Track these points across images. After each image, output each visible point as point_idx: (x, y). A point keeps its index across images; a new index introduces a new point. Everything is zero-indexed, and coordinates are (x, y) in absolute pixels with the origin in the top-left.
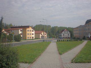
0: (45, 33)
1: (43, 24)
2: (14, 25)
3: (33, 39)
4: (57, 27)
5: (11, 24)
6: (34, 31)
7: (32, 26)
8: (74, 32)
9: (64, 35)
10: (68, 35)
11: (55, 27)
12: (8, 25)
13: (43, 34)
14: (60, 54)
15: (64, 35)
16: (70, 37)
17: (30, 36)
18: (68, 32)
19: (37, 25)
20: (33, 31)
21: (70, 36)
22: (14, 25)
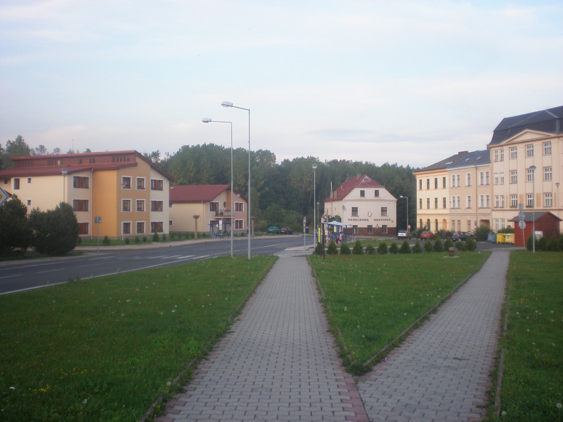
0: (235, 199)
1: (225, 140)
2: (42, 147)
3: (156, 239)
4: (312, 160)
5: (20, 139)
6: (166, 185)
7: (156, 155)
8: (506, 149)
9: (355, 211)
10: (384, 210)
11: (299, 162)
12: (14, 142)
13: (221, 207)
14: (358, 370)
15: (355, 211)
16: (392, 224)
17: (156, 217)
18: (384, 193)
19: (260, 151)
20: (157, 186)
21: (391, 221)
22: (42, 147)
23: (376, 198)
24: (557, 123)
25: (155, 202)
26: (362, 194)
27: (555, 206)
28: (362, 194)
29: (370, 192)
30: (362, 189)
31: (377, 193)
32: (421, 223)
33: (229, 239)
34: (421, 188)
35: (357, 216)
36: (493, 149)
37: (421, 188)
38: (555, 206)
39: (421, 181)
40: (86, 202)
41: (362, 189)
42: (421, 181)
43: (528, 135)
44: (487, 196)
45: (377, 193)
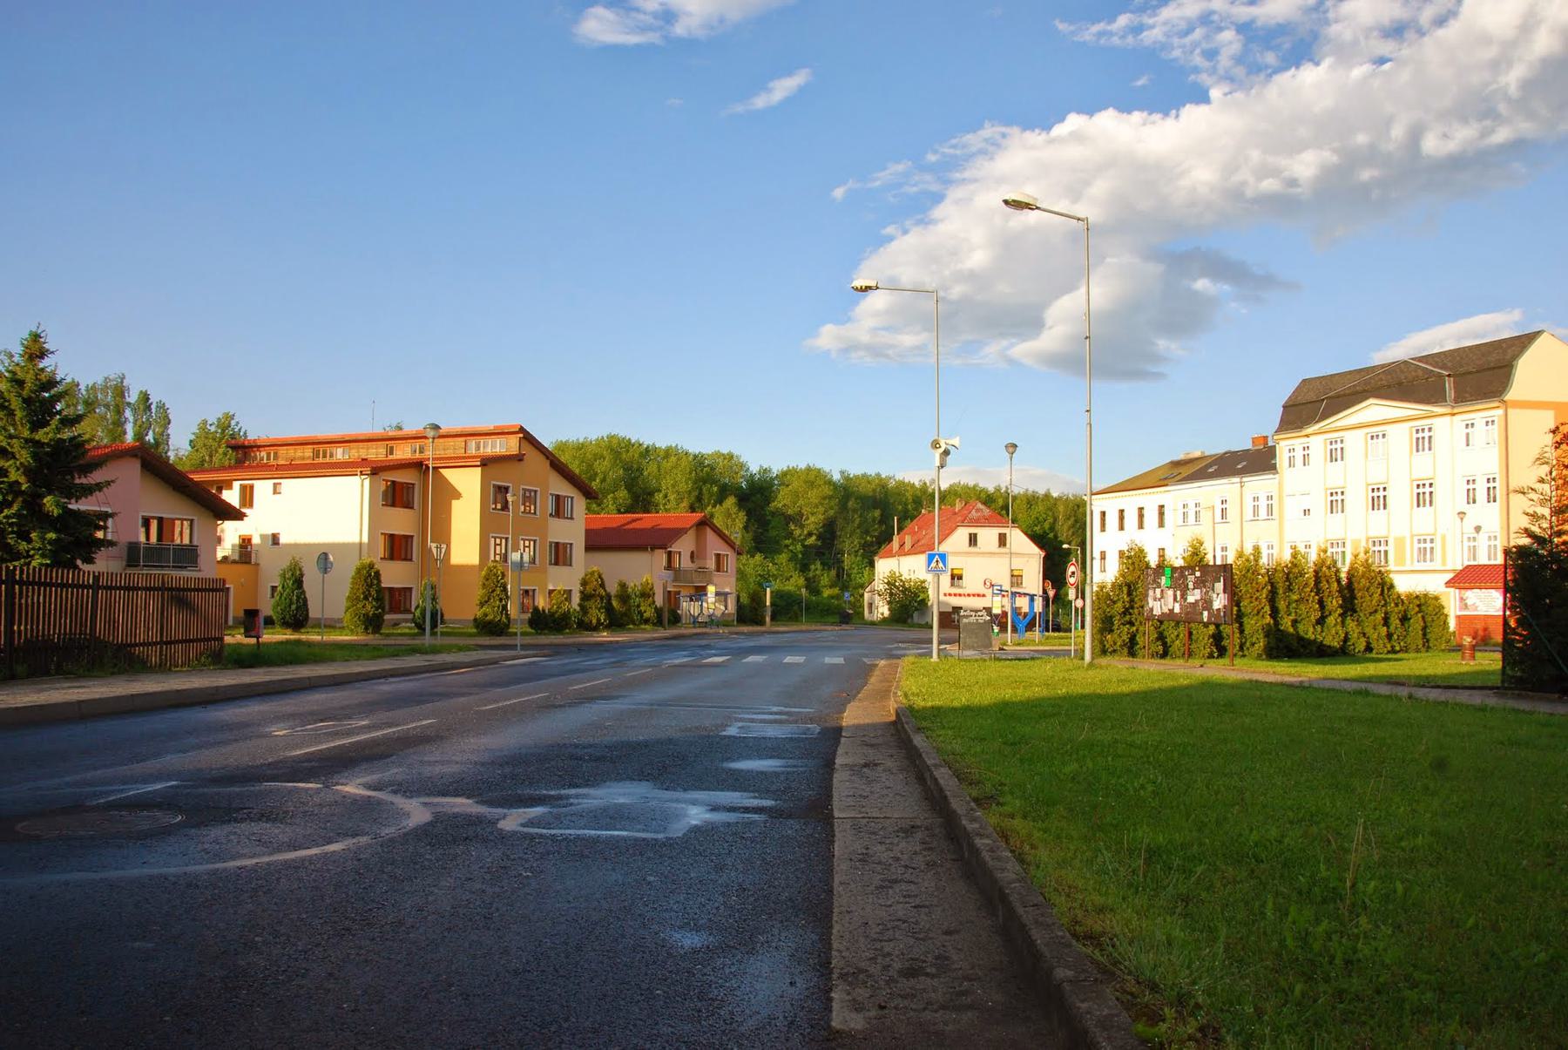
18: (1018, 539)
23: (973, 549)
24: (1449, 385)
25: (392, 536)
26: (973, 540)
27: (1444, 563)
28: (973, 540)
29: (988, 536)
30: (973, 530)
31: (1002, 540)
32: (577, 796)
33: (1408, 562)
34: (1103, 528)
35: (960, 587)
36: (1282, 443)
37: (1103, 528)
38: (1444, 563)
39: (1103, 514)
40: (408, 539)
41: (973, 530)
42: (1103, 514)
43: (1373, 410)
44: (1270, 498)
45: (1002, 540)
